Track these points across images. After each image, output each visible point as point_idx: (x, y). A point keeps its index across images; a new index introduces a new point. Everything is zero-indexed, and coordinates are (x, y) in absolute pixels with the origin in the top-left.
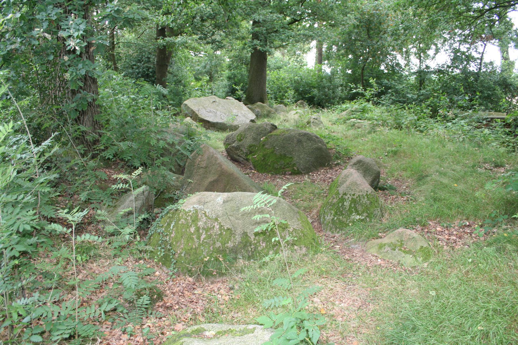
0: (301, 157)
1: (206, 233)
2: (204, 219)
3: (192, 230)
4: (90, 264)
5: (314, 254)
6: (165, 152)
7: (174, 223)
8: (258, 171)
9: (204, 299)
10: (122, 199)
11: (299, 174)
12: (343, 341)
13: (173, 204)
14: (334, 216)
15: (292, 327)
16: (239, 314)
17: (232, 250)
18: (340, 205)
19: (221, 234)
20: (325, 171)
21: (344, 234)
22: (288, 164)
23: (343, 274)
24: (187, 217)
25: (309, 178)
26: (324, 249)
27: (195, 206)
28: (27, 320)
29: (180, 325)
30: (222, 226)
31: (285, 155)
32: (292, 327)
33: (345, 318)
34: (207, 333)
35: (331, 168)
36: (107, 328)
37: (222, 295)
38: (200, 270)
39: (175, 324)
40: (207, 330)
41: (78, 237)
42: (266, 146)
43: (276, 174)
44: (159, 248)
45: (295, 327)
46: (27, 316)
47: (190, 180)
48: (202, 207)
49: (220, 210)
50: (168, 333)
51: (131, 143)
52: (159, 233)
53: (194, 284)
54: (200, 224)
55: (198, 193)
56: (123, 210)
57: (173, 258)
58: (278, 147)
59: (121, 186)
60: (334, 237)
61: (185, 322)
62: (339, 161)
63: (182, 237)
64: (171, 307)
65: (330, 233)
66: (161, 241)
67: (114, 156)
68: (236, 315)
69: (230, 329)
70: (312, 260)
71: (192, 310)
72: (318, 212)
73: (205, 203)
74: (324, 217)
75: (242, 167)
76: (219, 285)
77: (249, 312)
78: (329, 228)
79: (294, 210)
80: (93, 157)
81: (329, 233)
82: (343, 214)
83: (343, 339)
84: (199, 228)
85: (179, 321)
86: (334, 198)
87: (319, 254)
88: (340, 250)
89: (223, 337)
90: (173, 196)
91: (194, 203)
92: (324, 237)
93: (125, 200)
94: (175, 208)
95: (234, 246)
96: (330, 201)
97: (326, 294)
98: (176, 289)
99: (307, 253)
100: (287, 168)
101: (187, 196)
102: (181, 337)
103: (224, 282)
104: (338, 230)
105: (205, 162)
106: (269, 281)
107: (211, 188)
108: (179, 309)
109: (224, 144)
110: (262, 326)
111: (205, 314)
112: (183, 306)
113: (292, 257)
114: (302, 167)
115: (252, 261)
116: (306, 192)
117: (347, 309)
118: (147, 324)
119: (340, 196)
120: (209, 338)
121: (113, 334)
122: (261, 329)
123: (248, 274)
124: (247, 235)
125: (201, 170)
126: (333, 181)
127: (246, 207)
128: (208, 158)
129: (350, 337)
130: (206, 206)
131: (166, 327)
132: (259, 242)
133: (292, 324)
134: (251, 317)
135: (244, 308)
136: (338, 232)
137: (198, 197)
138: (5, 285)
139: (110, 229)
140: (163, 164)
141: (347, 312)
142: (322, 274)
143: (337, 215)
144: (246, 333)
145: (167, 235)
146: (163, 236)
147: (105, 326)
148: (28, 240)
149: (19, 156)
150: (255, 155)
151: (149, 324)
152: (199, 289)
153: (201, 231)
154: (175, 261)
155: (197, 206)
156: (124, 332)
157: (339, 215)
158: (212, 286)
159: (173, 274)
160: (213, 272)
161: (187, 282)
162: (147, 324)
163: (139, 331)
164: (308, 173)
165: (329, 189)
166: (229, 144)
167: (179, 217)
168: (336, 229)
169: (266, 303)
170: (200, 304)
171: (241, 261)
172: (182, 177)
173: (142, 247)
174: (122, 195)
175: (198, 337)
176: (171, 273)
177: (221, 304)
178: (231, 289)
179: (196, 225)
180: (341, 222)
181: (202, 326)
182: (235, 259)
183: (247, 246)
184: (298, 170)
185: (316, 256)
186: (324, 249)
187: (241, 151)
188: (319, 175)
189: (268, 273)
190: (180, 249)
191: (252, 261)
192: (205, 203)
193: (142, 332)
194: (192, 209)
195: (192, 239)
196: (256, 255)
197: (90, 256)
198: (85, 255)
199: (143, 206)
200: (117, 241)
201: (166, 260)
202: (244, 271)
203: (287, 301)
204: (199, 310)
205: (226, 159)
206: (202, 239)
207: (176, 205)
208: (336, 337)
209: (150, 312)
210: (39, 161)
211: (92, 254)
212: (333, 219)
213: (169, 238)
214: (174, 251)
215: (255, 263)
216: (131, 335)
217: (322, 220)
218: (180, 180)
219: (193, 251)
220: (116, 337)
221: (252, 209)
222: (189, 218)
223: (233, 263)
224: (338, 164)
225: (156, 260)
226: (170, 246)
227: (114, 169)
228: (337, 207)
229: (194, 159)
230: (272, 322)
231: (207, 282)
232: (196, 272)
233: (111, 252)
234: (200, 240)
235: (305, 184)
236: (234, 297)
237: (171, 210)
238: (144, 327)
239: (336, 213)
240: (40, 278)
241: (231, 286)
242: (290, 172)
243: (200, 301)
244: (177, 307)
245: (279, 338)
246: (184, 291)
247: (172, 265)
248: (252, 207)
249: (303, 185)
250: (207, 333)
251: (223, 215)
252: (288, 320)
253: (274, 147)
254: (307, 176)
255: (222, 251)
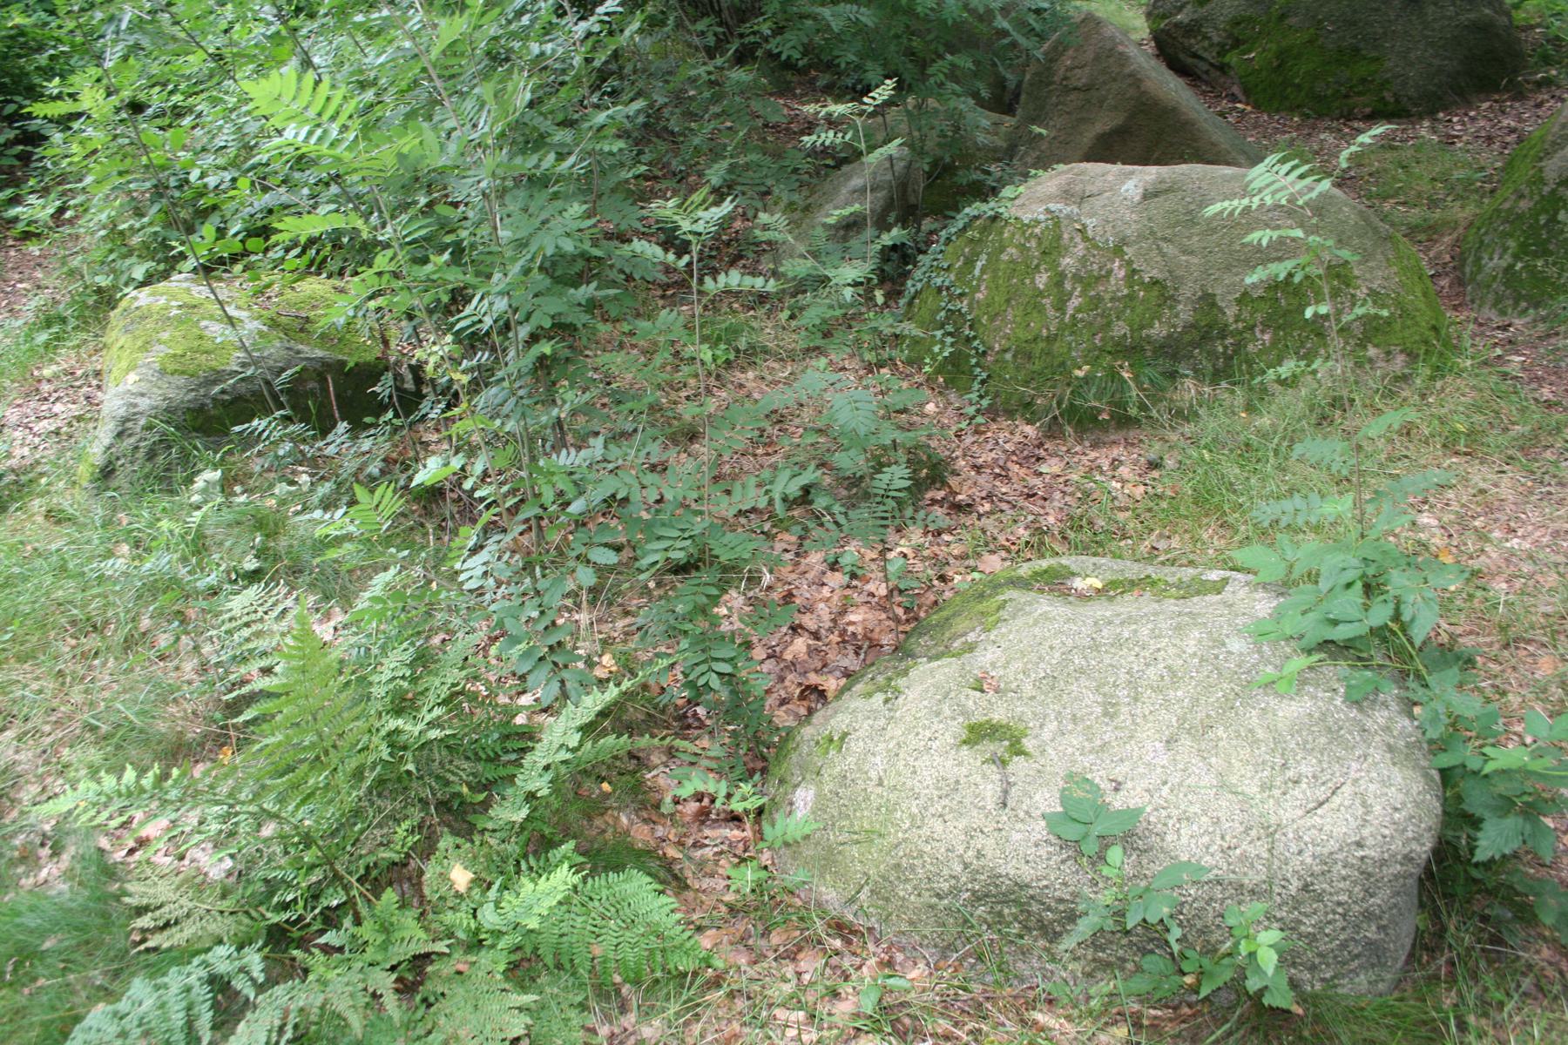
0: (1412, 56)
1: (1083, 293)
2: (1080, 249)
3: (1042, 280)
4: (738, 374)
5: (1432, 378)
6: (960, 37)
7: (984, 257)
8: (1257, 106)
9: (1069, 490)
10: (827, 186)
11: (1400, 117)
12: (1506, 653)
13: (985, 201)
14: (1516, 257)
15: (1349, 585)
16: (1175, 542)
17: (1162, 347)
18: (1543, 219)
19: (1131, 297)
20: (1496, 106)
21: (1544, 320)
22: (1363, 81)
23: (1529, 446)
24: (1028, 239)
25: (1434, 130)
26: (1469, 363)
27: (1052, 206)
28: (576, 507)
29: (995, 558)
30: (1134, 271)
31: (1356, 50)
32: (1349, 585)
33: (1518, 583)
34: (1078, 583)
35: (1520, 96)
36: (786, 551)
37: (1123, 481)
38: (1059, 404)
39: (979, 555)
40: (1078, 575)
41: (708, 279)
42: (1292, 21)
43: (1320, 116)
44: (939, 333)
45: (1359, 585)
46: (576, 498)
47: (1037, 129)
48: (1076, 210)
49: (1131, 223)
50: (958, 578)
51: (855, 8)
52: (939, 290)
53: (1041, 445)
54: (1067, 262)
55: (1061, 167)
56: (837, 212)
57: (977, 365)
58: (1333, 23)
59: (828, 137)
60: (1504, 328)
61: (1008, 551)
62: (1554, 72)
63: (1008, 301)
64: (969, 505)
65: (1493, 314)
66: (943, 314)
67: (804, 54)
68: (1162, 545)
69: (1148, 577)
70: (1423, 396)
71: (1031, 518)
72: (1457, 243)
73: (1083, 198)
74: (1479, 259)
75: (1204, 93)
76: (1116, 452)
77: (1205, 536)
78: (1491, 297)
79: (1375, 230)
80: (741, 59)
81: (1488, 313)
82: (1546, 253)
83: (1506, 646)
84: (1062, 275)
85: (992, 547)
86: (1522, 196)
87: (1449, 379)
88: (1524, 369)
89: (1127, 597)
90: (982, 177)
91: (1050, 198)
92: (1471, 326)
93: (836, 190)
94: (991, 213)
95: (1170, 336)
96: (1507, 205)
97: (1463, 506)
98: (985, 457)
99: (1406, 371)
100: (1360, 94)
101: (1026, 176)
102: (1000, 585)
103: (1133, 445)
104: (1524, 304)
105: (1087, 70)
106: (1276, 452)
107: (1107, 149)
108: (991, 513)
109: (1149, 15)
110: (1251, 577)
111: (1071, 535)
112: (1004, 506)
113: (1356, 382)
114: (1412, 92)
115: (1224, 384)
116: (1421, 177)
117: (1531, 557)
118: (899, 549)
119: (1546, 190)
120: (1082, 597)
121: (802, 568)
122: (1247, 584)
123: (1210, 424)
124: (1214, 304)
125: (1073, 96)
126: (1520, 140)
127: (1226, 204)
128: (1097, 58)
129: (1529, 642)
130: (1086, 207)
131: (952, 561)
132: (1252, 328)
133: (1350, 575)
134: (1211, 551)
135: (1189, 524)
136: (1524, 312)
137: (1063, 179)
138: (519, 410)
139: (798, 269)
140: (953, 75)
141: (1526, 568)
142: (1455, 442)
143: (1526, 254)
144: (1198, 593)
145: (961, 295)
146: (951, 298)
147: (779, 546)
148: (572, 291)
149: (535, 48)
150: (1250, 52)
151: (905, 550)
152: (1054, 461)
153: (1068, 286)
154: (984, 375)
155: (1059, 206)
156: (834, 566)
157: (1536, 255)
158: (1093, 455)
159: (978, 411)
160: (1100, 411)
161: (1018, 438)
162: (899, 549)
163: (874, 567)
164: (1431, 113)
165: (1503, 169)
166: (1164, 17)
167: (1001, 241)
168: (1516, 303)
169: (1266, 511)
170: (1056, 504)
171: (1189, 383)
172: (1009, 121)
173: (886, 324)
174: (827, 175)
175: (1051, 590)
176: (971, 410)
177: (1120, 509)
178: (1154, 465)
179: (1054, 265)
180: (1538, 279)
181: (1064, 561)
182: (1173, 376)
183: (1211, 339)
184: (1397, 101)
185: (1439, 384)
186: (1469, 363)
187: (1206, 37)
188: (1468, 125)
189: (1272, 425)
190: (1004, 334)
191: (1224, 384)
192: (1083, 198)
193: (884, 570)
194: (1042, 217)
195: (1040, 309)
196: (1240, 370)
197: (737, 351)
198: (723, 346)
199: (888, 206)
200: (817, 310)
201: (955, 372)
202: (1197, 415)
203: (1339, 506)
204: (1051, 520)
205: (1154, 62)
206: (1070, 312)
207: (992, 204)
208: (1481, 639)
209: (909, 512)
210: (593, 59)
211: (742, 344)
212: (1511, 266)
213: (970, 305)
214: (983, 343)
215: (1233, 392)
216: (853, 576)
217: (1467, 270)
218: (1003, 129)
219: (1042, 345)
220: (810, 576)
221: (1247, 210)
222: (1033, 243)
223: (1163, 389)
224: (1547, 83)
225: (927, 369)
226: (971, 327)
227: (802, 95)
228: (1531, 226)
229: (1051, 61)
230: (1284, 564)
231: (1080, 441)
232: (1048, 410)
233: (799, 341)
234: (1064, 314)
235: (1417, 149)
236: (1159, 491)
237: (976, 218)
238: (891, 555)
239: (1523, 247)
240: (604, 405)
241: (1152, 456)
242: (1368, 110)
243: (1057, 495)
244: (987, 507)
245: (1304, 613)
246: (1009, 464)
247: (976, 386)
248: (1246, 202)
249: (1410, 153)
250: (1078, 583)
251: (1141, 237)
252: (1340, 564)
253: (1320, 22)
254: (1426, 123)
255: (1130, 350)
